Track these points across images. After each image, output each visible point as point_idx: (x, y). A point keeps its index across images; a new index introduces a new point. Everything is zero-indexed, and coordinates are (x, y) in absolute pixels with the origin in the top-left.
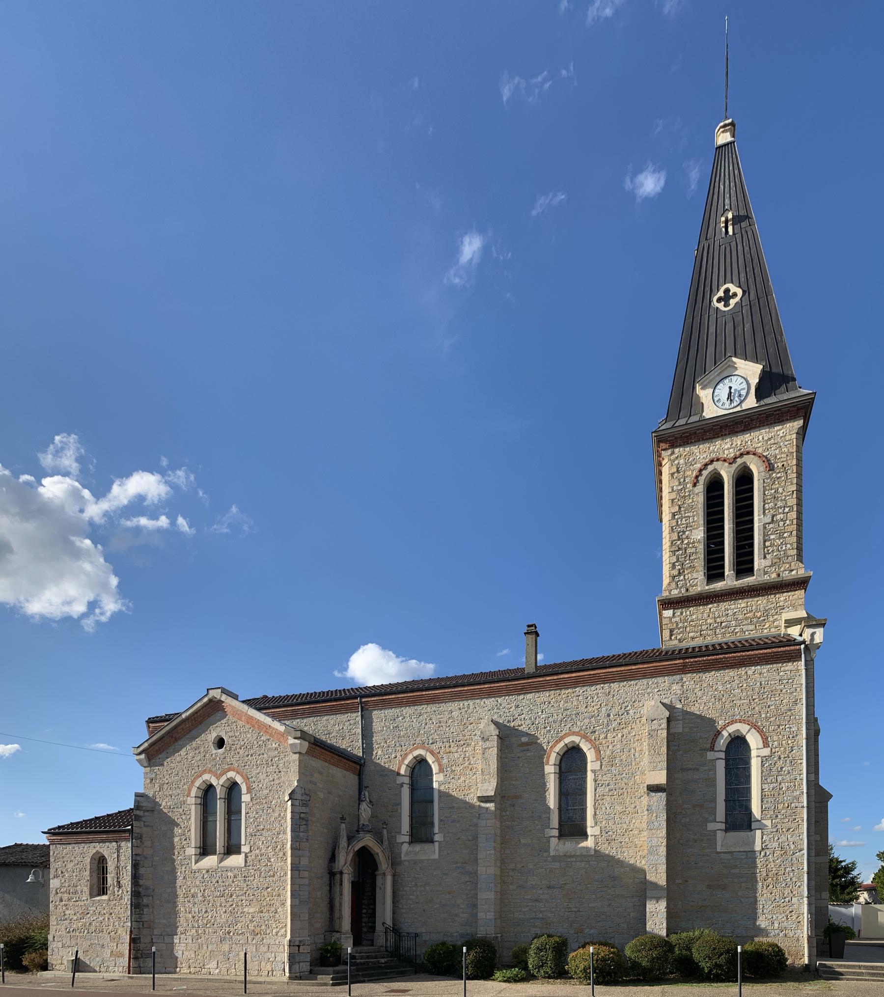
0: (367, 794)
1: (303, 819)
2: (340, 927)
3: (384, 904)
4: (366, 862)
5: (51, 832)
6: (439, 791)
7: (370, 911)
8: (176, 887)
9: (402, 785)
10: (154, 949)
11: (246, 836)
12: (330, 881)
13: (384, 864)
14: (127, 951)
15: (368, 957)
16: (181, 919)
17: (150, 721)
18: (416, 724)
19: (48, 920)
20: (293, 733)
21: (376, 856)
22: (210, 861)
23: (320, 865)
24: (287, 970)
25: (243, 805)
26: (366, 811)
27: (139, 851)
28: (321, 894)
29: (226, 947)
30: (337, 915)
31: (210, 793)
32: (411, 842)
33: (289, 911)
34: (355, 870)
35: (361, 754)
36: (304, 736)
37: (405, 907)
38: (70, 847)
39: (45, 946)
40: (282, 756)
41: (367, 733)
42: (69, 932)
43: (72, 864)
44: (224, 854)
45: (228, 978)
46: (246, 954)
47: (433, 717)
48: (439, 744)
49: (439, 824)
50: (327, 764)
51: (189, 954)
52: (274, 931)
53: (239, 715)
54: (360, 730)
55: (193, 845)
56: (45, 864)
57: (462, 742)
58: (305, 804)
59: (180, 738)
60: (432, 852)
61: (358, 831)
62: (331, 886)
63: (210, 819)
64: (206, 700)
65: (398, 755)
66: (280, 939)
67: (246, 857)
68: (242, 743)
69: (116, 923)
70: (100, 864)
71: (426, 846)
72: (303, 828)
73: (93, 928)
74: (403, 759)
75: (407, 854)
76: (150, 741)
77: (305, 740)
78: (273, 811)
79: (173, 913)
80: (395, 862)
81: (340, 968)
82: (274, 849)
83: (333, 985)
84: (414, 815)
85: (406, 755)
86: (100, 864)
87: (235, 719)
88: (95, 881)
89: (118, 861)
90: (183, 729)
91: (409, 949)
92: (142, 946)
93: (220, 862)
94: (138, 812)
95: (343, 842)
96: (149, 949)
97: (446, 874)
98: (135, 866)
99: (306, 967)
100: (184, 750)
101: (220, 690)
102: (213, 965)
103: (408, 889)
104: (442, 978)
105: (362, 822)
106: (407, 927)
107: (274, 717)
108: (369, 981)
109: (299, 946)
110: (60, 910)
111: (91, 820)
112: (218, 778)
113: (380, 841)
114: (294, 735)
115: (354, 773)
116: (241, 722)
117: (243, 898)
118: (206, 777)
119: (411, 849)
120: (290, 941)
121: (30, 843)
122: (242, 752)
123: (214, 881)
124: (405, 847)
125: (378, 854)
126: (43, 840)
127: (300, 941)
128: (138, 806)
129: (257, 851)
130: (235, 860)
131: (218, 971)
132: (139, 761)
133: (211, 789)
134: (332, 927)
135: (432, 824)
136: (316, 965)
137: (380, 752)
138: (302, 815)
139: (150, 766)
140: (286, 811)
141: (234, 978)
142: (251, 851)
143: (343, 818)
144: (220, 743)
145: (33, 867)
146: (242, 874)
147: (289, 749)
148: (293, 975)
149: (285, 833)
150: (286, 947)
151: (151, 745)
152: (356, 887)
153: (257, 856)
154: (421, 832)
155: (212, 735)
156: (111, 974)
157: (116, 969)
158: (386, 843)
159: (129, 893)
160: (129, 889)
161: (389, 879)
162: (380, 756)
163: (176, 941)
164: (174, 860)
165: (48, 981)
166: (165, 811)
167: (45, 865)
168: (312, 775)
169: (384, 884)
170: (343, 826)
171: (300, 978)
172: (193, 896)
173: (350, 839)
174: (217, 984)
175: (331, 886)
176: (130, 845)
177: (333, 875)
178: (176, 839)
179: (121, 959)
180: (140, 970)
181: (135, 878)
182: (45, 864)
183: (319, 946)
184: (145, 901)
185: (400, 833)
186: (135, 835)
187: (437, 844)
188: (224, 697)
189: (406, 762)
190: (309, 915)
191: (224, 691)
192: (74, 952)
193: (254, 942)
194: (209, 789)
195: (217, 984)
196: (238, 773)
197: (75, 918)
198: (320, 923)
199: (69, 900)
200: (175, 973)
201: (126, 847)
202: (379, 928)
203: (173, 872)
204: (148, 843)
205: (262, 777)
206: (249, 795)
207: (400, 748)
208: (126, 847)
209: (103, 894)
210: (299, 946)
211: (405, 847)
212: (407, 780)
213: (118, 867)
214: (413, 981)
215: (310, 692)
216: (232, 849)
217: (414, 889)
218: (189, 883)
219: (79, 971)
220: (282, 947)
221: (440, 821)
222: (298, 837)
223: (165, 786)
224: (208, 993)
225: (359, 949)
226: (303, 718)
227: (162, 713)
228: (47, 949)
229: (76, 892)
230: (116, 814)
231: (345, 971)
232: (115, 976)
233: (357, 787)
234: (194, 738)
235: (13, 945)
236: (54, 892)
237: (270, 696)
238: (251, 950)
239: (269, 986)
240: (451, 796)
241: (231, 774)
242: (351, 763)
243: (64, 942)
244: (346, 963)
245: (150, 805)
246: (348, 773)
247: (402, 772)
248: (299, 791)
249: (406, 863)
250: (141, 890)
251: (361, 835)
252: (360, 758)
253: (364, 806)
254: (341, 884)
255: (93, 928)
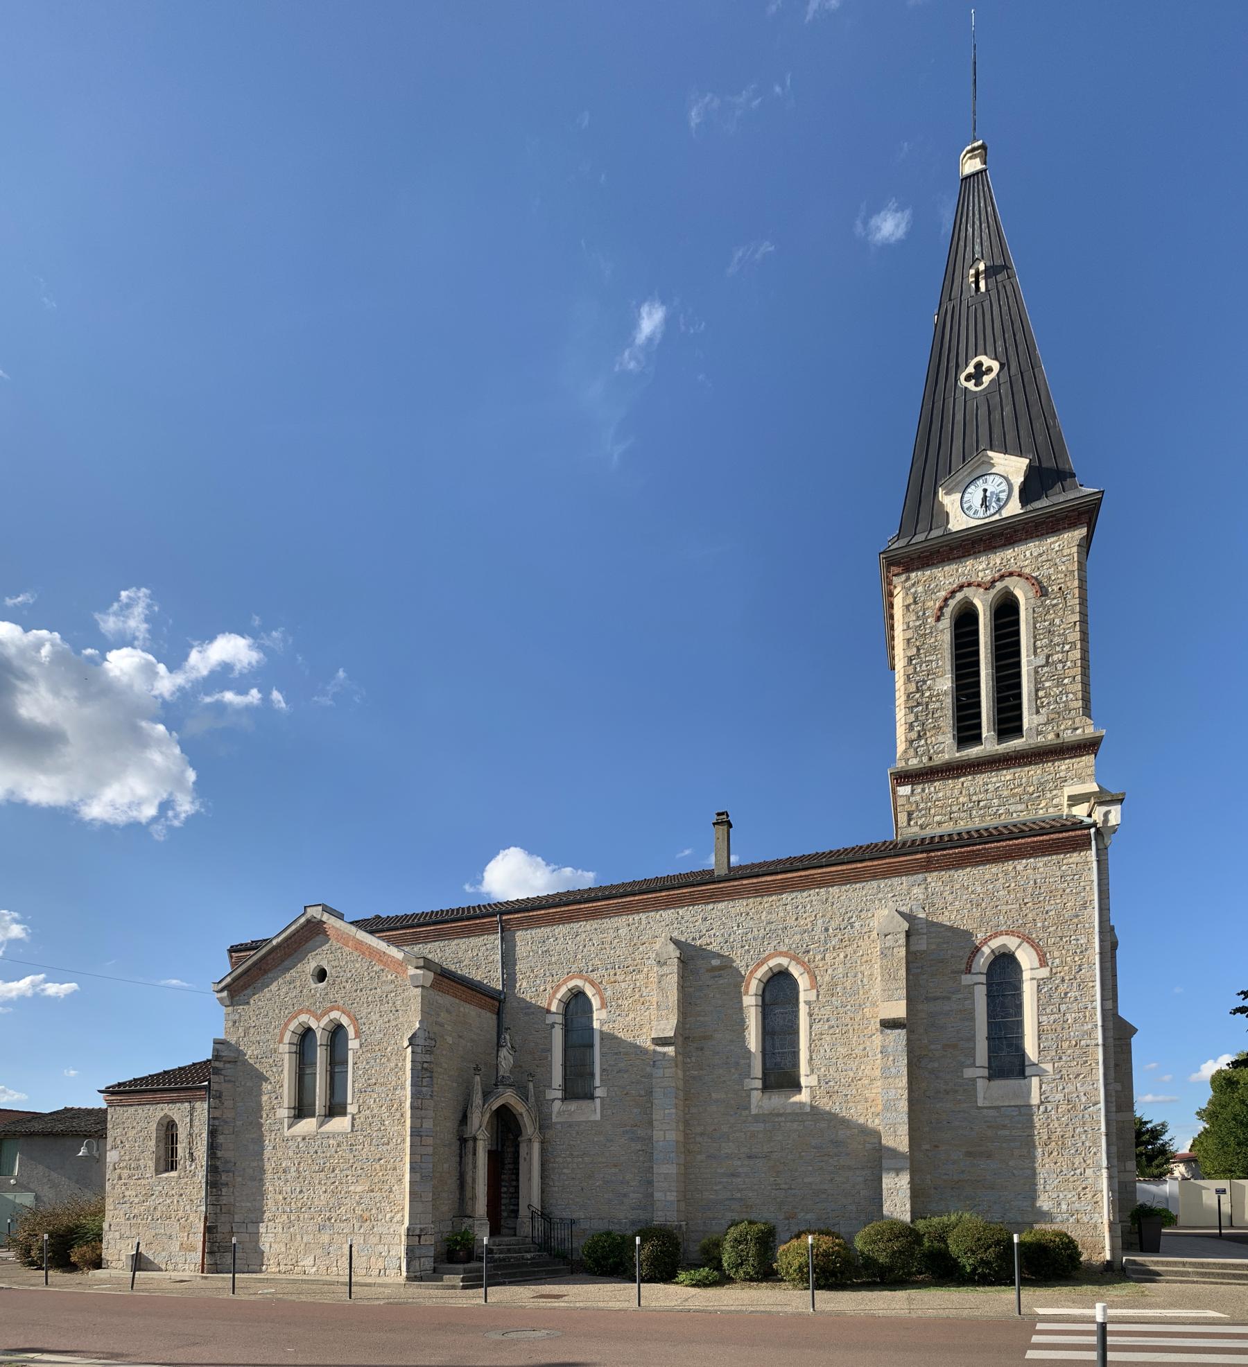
29: (325, 1238)
200: (261, 1271)
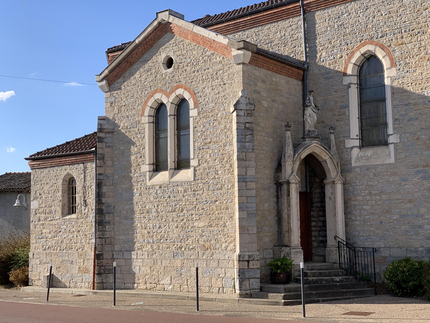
0: (312, 98)
1: (248, 129)
2: (290, 241)
3: (335, 215)
4: (313, 169)
5: (32, 158)
6: (392, 88)
7: (320, 224)
8: (132, 204)
9: (349, 86)
10: (115, 264)
11: (194, 150)
12: (277, 192)
13: (332, 172)
14: (92, 267)
15: (320, 274)
16: (138, 235)
17: (110, 51)
18: (362, 19)
19: (29, 239)
20: (237, 45)
21: (323, 164)
22: (163, 177)
23: (267, 173)
24: (237, 287)
25: (191, 120)
26: (311, 117)
27: (101, 171)
28: (269, 206)
29: (178, 263)
30: (285, 228)
31: (161, 112)
32: (361, 147)
33: (237, 225)
34: (302, 180)
35: (304, 59)
36: (246, 46)
37: (359, 218)
38: (47, 170)
39: (26, 263)
40: (226, 68)
41: (310, 37)
42: (45, 250)
43: (48, 186)
44: (175, 169)
45: (181, 294)
46: (197, 269)
47: (382, 9)
48: (389, 37)
49: (394, 124)
50: (270, 73)
51: (146, 270)
52: (224, 245)
53: (185, 33)
54: (302, 35)
55: (147, 162)
56: (27, 190)
57: (416, 31)
58: (250, 114)
59: (134, 63)
60: (387, 156)
61: (303, 138)
62: (278, 197)
63: (162, 136)
64: (156, 23)
65: (344, 55)
66: (229, 254)
67: (195, 170)
68: (189, 60)
69: (83, 241)
70: (70, 185)
71: (380, 150)
72: (248, 138)
73: (64, 245)
74: (350, 58)
75: (358, 159)
76: (110, 68)
77: (247, 49)
78: (219, 123)
79: (132, 229)
80: (344, 168)
81: (291, 286)
82: (221, 161)
83: (286, 304)
84: (364, 117)
85: (353, 53)
86: (70, 185)
87: (182, 39)
88: (66, 200)
89: (85, 181)
90: (137, 54)
91: (366, 267)
92: (105, 262)
93: (172, 177)
94: (100, 135)
95: (289, 150)
96: (109, 270)
97: (406, 180)
98: (99, 185)
99: (256, 284)
100: (138, 73)
101: (167, 13)
102: (166, 281)
103: (361, 198)
104: (406, 299)
105: (307, 128)
106: (365, 239)
107: (217, 31)
108: (324, 301)
109: (248, 261)
110: (38, 229)
111: (63, 145)
112: (168, 97)
113: (328, 147)
114: (237, 47)
115: (297, 79)
116: (189, 40)
117: (193, 212)
118: (158, 96)
119: (362, 154)
120: (239, 256)
121: (17, 172)
122: (188, 69)
123: (166, 196)
124: (355, 152)
125: (325, 161)
126: (24, 167)
127: (249, 256)
128: (100, 129)
129: (205, 165)
130: (185, 175)
131: (171, 287)
132: (101, 87)
133: (163, 108)
134: (281, 241)
135: (385, 125)
136: (266, 282)
137: (324, 54)
138: (247, 125)
139: (110, 91)
140: (231, 122)
141: (186, 294)
142: (199, 165)
143: (288, 126)
144: (169, 63)
145: (18, 192)
146: (191, 187)
147: (232, 61)
148: (244, 292)
149: (231, 144)
150: (236, 263)
151: (110, 72)
152: (305, 198)
153: (205, 169)
154: (373, 134)
155: (162, 57)
156: (79, 290)
157: (83, 285)
158: (334, 148)
159: (94, 211)
160: (94, 207)
161: (339, 188)
162: (325, 58)
163: (134, 257)
164: (131, 178)
165: (29, 295)
166: (123, 131)
167: (27, 191)
168: (256, 85)
169: (334, 193)
170: (288, 133)
171: (251, 296)
172: (148, 212)
173: (296, 147)
174: (171, 301)
175: (278, 198)
176: (94, 165)
177: (280, 186)
178: (133, 158)
179: (87, 275)
180: (102, 286)
181: (99, 196)
182: (27, 190)
183: (268, 261)
184: (107, 218)
185: (349, 137)
186: (98, 156)
187: (392, 147)
188: (171, 19)
189: (353, 60)
190: (258, 228)
191: (172, 13)
192: (49, 268)
193: (204, 257)
194: (161, 107)
195: (171, 301)
196: (186, 89)
197: (50, 236)
198: (268, 239)
199: (45, 219)
200: (133, 288)
201: (91, 167)
202: (331, 242)
203: (130, 190)
204: (109, 163)
205: (207, 91)
206: (196, 110)
207: (346, 47)
208: (91, 167)
209: (73, 212)
210: (248, 261)
211: (355, 152)
212: (355, 80)
213: (84, 187)
214: (374, 303)
215: (250, 5)
216: (182, 164)
217: (368, 198)
218: (144, 199)
219: (53, 287)
220: (231, 262)
221: (395, 120)
222: (244, 147)
223: (123, 108)
224: (164, 309)
225: (310, 265)
226: (244, 30)
227: (119, 44)
228: (28, 266)
229: (50, 212)
230: (83, 138)
231: (297, 290)
232: (82, 291)
233: (301, 92)
234: (63, 193)
235: (3, 262)
236: (34, 213)
237: (212, 15)
238: (202, 266)
239: (221, 304)
240: (406, 91)
241: (179, 91)
242: (294, 69)
243: (41, 258)
244: (297, 281)
245: (110, 127)
246: (291, 80)
247: (349, 72)
248: (243, 101)
249: (358, 170)
250: (103, 207)
251: (308, 141)
252: (304, 63)
253: (309, 111)
254: (289, 195)
255: (64, 245)
